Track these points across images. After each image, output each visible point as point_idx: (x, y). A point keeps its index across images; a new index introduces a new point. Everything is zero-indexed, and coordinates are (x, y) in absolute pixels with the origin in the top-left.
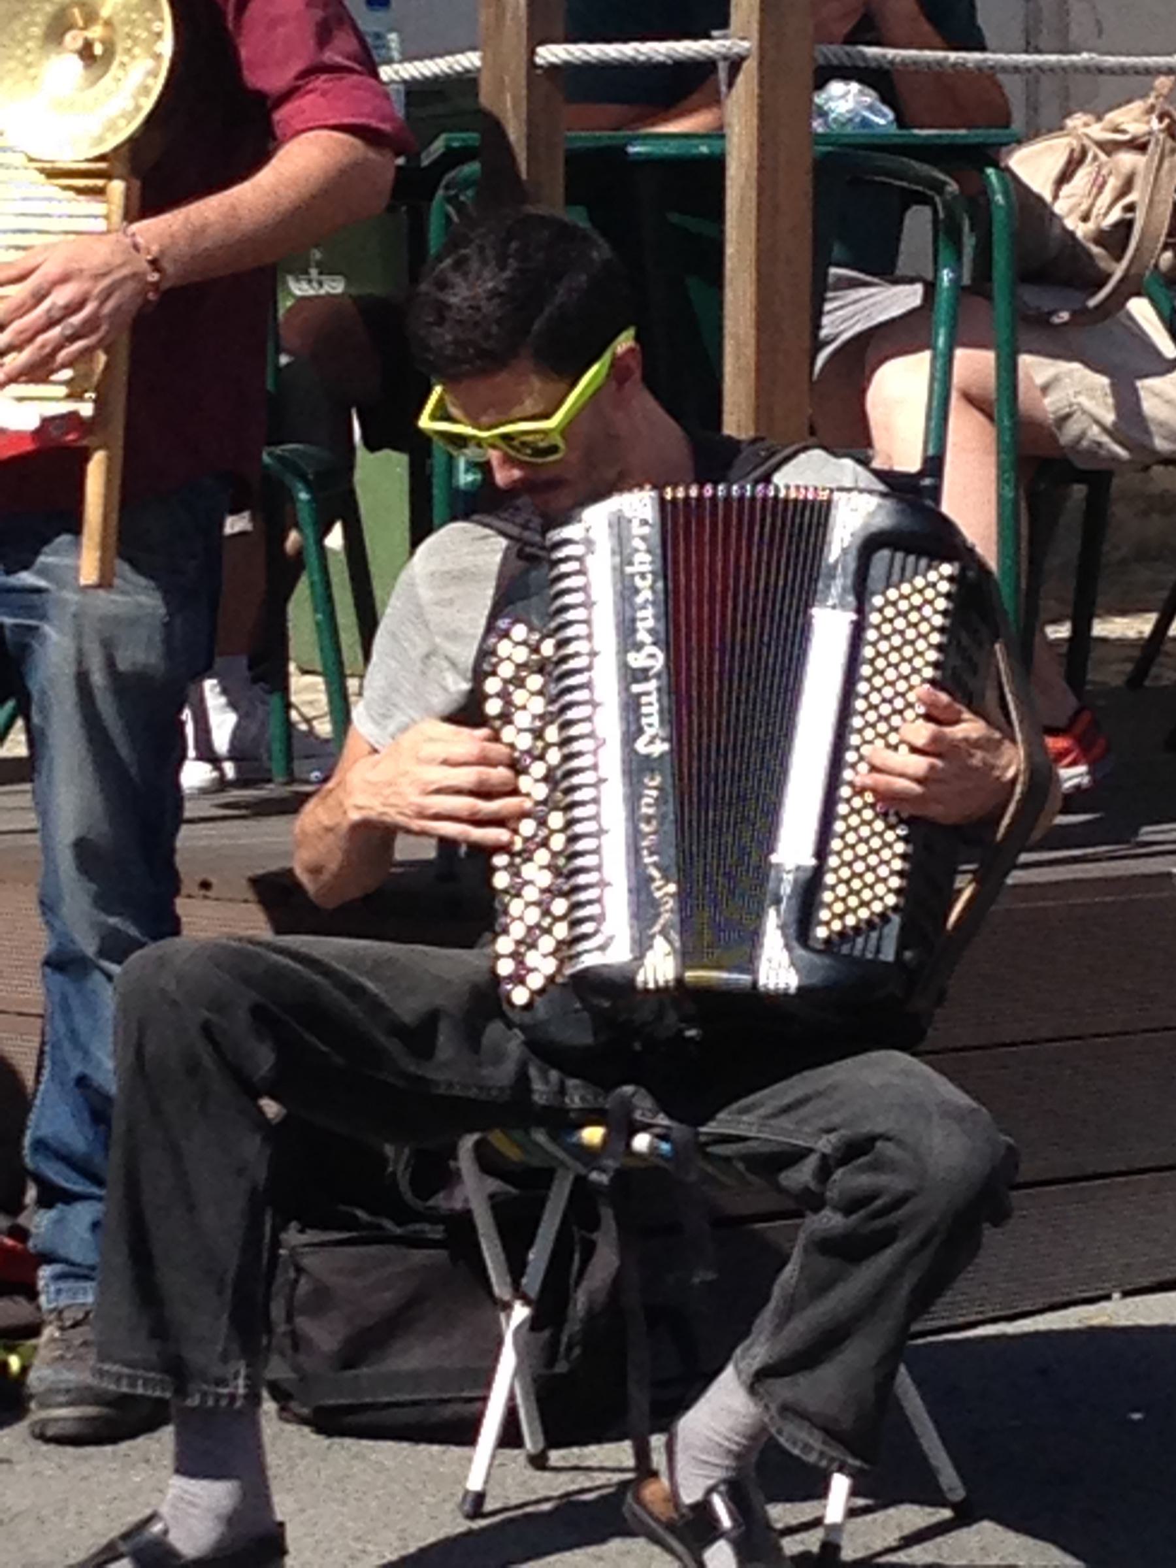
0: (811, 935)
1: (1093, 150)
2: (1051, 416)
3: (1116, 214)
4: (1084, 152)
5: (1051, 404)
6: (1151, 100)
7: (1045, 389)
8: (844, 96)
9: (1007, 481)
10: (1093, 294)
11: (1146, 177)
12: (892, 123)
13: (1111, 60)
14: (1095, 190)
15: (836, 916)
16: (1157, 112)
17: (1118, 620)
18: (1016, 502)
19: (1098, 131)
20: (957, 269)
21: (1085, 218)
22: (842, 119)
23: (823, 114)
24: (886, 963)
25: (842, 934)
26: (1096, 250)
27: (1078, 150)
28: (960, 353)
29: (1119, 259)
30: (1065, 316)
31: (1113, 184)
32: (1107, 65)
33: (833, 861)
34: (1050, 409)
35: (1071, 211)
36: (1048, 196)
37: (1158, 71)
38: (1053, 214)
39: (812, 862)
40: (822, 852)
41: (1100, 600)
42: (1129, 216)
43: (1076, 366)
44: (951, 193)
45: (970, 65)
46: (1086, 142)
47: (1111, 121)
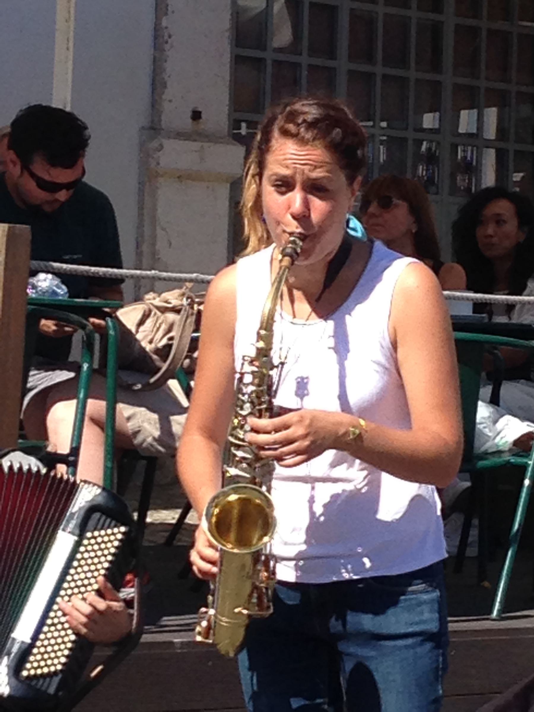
0: (20, 675)
1: (155, 310)
2: (131, 431)
3: (164, 341)
4: (150, 311)
5: (131, 426)
6: (183, 290)
7: (129, 419)
8: (45, 280)
9: (109, 454)
10: (152, 376)
11: (179, 325)
12: (66, 293)
13: (164, 274)
14: (155, 329)
15: (33, 668)
16: (186, 296)
17: (164, 512)
18: (112, 468)
19: (157, 302)
20: (91, 363)
21: (151, 342)
22: (44, 291)
23: (34, 287)
24: (49, 695)
25: (35, 676)
26: (155, 357)
27: (147, 310)
28: (90, 401)
29: (165, 361)
30: (139, 386)
31: (164, 327)
32: (163, 276)
33: (39, 643)
34: (130, 428)
35: (145, 337)
36: (133, 330)
37: (186, 280)
38: (136, 340)
39: (29, 641)
40: (35, 638)
41: (151, 501)
42: (170, 342)
43: (143, 409)
44: (89, 329)
45: (101, 274)
46: (152, 307)
47: (165, 297)
